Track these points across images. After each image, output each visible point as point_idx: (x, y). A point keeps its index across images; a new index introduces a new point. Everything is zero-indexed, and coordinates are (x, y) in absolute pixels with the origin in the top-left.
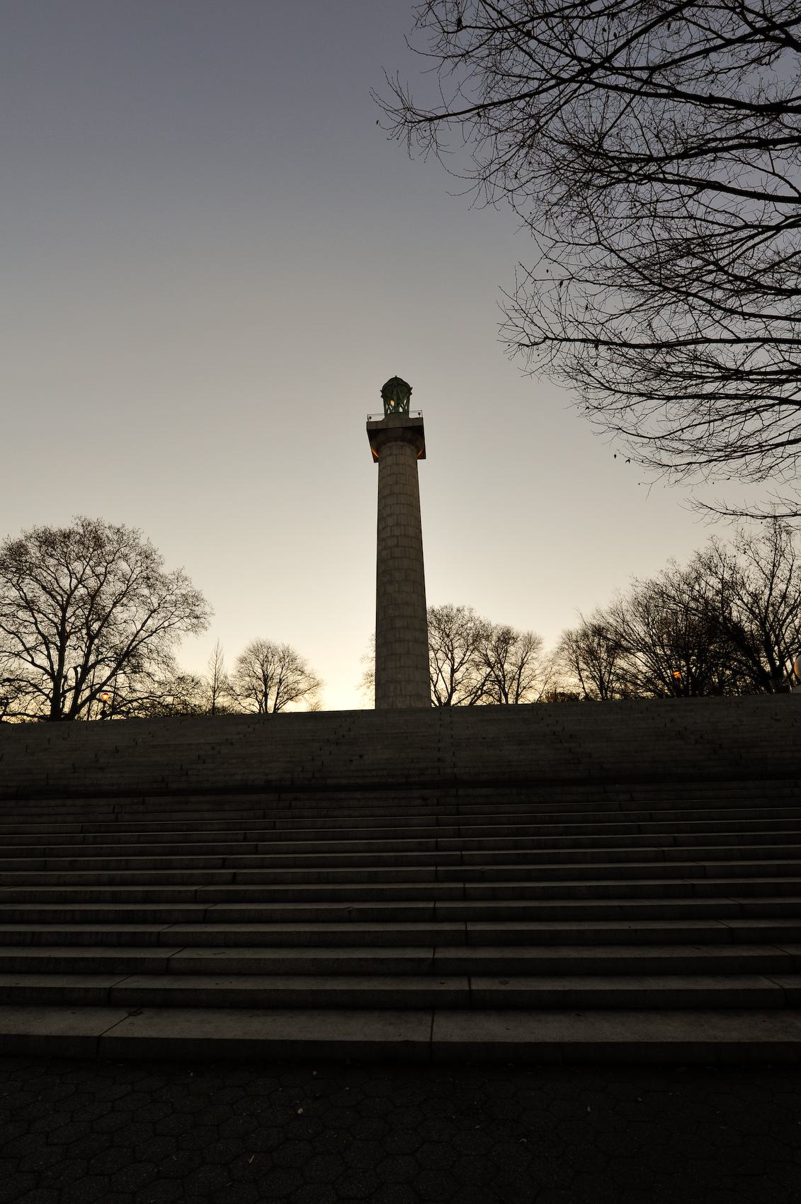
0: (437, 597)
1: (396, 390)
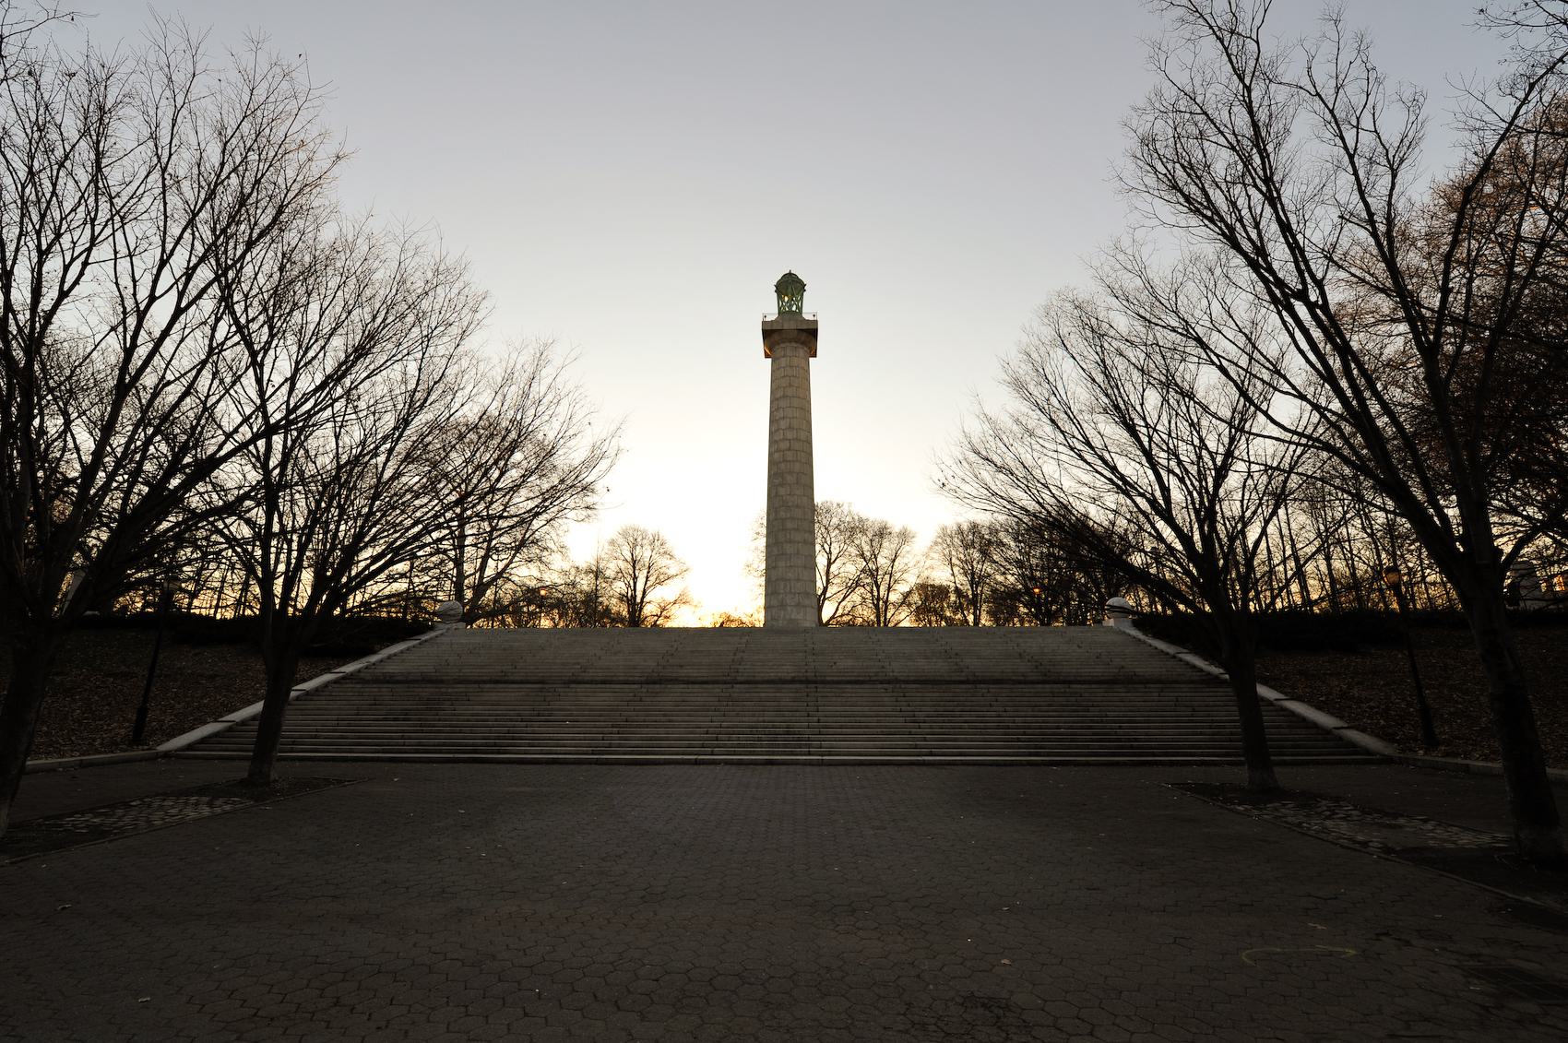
0: (823, 493)
1: (790, 287)
